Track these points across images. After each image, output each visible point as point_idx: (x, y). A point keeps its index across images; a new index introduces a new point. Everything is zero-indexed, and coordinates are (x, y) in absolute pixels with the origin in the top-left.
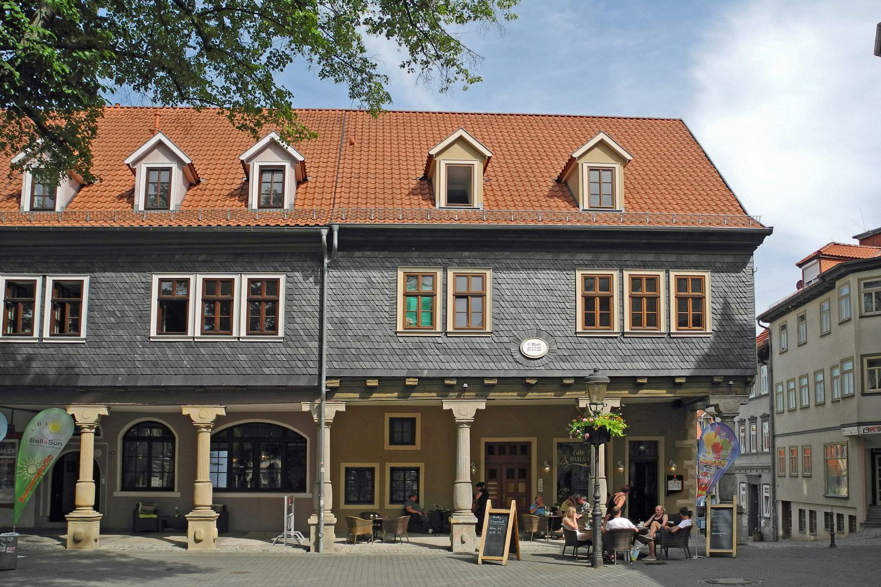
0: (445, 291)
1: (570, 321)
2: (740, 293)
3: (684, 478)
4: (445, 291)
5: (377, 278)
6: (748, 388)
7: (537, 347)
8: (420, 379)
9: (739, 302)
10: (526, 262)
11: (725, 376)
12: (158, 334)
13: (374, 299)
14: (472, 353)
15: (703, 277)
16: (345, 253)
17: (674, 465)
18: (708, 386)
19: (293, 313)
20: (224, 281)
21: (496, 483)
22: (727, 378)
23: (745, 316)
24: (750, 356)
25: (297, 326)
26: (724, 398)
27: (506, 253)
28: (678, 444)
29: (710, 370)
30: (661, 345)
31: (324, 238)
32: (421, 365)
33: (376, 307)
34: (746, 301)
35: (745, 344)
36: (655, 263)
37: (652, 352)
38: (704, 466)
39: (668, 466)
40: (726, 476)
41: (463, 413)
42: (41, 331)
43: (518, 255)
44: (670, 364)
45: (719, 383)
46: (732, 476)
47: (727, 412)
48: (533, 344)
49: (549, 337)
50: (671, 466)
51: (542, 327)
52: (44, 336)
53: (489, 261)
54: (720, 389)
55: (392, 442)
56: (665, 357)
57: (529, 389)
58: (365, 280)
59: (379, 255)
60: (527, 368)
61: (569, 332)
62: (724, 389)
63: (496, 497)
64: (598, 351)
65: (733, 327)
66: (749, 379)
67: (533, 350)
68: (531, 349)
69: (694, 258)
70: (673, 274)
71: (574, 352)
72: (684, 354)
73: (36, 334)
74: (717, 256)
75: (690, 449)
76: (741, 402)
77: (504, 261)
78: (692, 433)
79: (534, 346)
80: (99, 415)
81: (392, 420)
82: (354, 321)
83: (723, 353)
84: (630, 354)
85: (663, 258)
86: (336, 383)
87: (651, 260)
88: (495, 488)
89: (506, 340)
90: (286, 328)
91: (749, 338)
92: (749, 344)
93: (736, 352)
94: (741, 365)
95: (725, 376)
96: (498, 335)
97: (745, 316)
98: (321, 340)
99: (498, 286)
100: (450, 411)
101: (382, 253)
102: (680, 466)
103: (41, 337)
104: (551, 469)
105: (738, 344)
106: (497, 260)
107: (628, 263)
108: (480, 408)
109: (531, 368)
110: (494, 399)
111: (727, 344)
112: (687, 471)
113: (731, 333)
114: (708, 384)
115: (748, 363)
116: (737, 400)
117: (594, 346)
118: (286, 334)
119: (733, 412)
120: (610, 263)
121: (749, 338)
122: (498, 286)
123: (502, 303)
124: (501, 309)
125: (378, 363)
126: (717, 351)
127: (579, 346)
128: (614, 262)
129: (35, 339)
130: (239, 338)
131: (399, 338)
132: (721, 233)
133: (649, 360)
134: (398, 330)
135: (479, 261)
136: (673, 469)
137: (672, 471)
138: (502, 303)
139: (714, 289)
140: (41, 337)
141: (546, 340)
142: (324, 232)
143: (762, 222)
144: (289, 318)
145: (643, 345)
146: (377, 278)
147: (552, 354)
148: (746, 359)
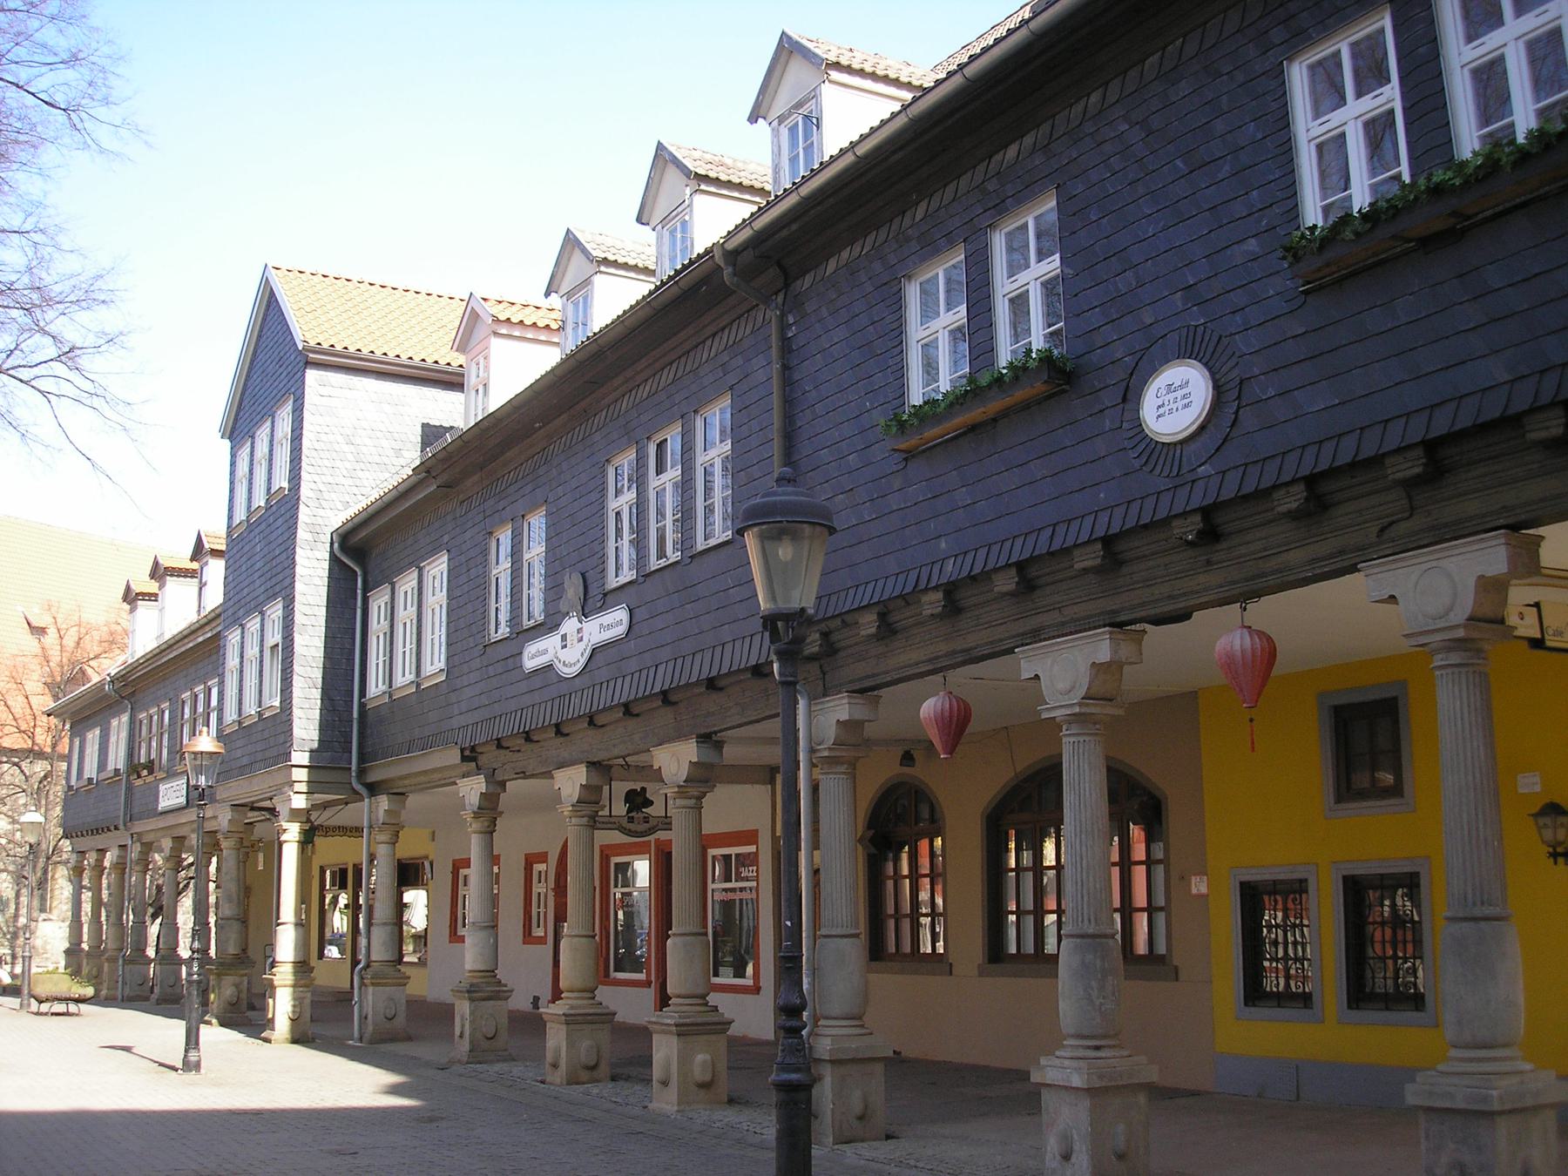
7: (1180, 393)
68: (1166, 408)
79: (1171, 396)
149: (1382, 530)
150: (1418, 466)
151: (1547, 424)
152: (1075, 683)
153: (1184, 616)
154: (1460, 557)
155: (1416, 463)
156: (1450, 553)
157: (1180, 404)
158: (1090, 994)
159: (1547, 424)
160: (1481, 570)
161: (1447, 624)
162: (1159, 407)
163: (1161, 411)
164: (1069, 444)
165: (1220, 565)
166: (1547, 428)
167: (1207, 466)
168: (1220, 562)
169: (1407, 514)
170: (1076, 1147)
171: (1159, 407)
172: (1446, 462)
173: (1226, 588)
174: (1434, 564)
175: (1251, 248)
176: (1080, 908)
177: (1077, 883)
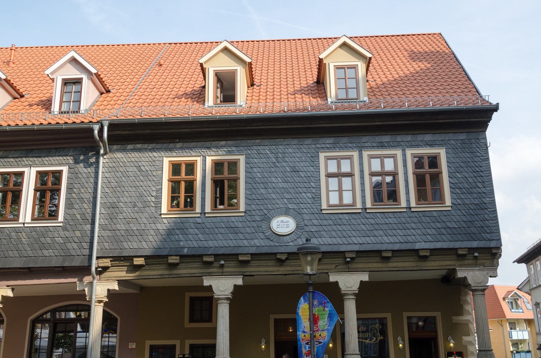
1: (316, 199)
2: (476, 168)
3: (465, 355)
5: (146, 167)
7: (285, 224)
8: (182, 257)
9: (476, 175)
10: (275, 148)
11: (469, 248)
12: (212, 210)
13: (142, 185)
14: (228, 232)
15: (396, 155)
16: (119, 146)
17: (452, 341)
18: (164, 267)
19: (72, 200)
20: (54, 172)
22: (471, 250)
23: (483, 189)
24: (492, 228)
25: (75, 212)
26: (472, 270)
27: (257, 141)
28: (455, 319)
29: (453, 243)
30: (403, 219)
31: (96, 132)
32: (182, 243)
33: (144, 192)
34: (482, 175)
35: (486, 216)
36: (391, 143)
37: (394, 226)
38: (306, 344)
39: (447, 341)
40: (483, 352)
41: (221, 289)
42: (408, 201)
43: (266, 142)
44: (413, 237)
45: (464, 256)
46: (489, 352)
47: (477, 285)
48: (282, 221)
49: (297, 214)
50: (449, 343)
51: (290, 206)
52: (206, 211)
53: (242, 148)
54: (467, 262)
55: (192, 320)
56: (408, 231)
57: (281, 265)
58: (135, 169)
59: (148, 146)
60: (277, 244)
61: (315, 210)
62: (470, 262)
64: (398, 225)
65: (472, 200)
66: (494, 251)
67: (282, 227)
68: (280, 226)
69: (428, 137)
70: (409, 152)
71: (320, 228)
72: (426, 227)
73: (198, 209)
74: (450, 134)
75: (467, 325)
76: (490, 275)
77: (255, 147)
78: (467, 309)
79: (283, 224)
80: (109, 290)
81: (192, 299)
82: (124, 205)
83: (465, 226)
84: (373, 229)
85: (399, 138)
86: (107, 262)
87: (388, 141)
89: (258, 218)
90: (66, 213)
91: (489, 210)
92: (491, 216)
93: (478, 224)
95: (469, 248)
96: (251, 214)
97: (483, 189)
98: (93, 223)
99: (250, 170)
100: (336, 283)
101: (151, 145)
102: (458, 341)
103: (203, 213)
104: (404, 345)
105: (479, 216)
106: (249, 147)
107: (366, 145)
108: (364, 280)
109: (281, 245)
110: (253, 275)
111: (467, 216)
112: (466, 347)
114: (378, 259)
116: (485, 273)
117: (339, 221)
118: (65, 218)
119: (482, 284)
120: (350, 145)
121: (489, 210)
122: (250, 170)
123: (254, 185)
124: (253, 190)
125: (144, 243)
126: (458, 223)
127: (325, 222)
128: (354, 144)
129: (60, 223)
130: (24, 224)
131: (163, 219)
133: (392, 234)
134: (162, 212)
135: (234, 149)
136: (452, 345)
137: (451, 347)
138: (254, 185)
139: (450, 165)
140: (203, 213)
141: (294, 218)
142: (96, 128)
143: (490, 101)
144: (69, 205)
145: (386, 220)
146: (146, 167)
147: (300, 230)
148: (489, 231)
149: (335, 267)
163: (278, 226)
174: (349, 276)
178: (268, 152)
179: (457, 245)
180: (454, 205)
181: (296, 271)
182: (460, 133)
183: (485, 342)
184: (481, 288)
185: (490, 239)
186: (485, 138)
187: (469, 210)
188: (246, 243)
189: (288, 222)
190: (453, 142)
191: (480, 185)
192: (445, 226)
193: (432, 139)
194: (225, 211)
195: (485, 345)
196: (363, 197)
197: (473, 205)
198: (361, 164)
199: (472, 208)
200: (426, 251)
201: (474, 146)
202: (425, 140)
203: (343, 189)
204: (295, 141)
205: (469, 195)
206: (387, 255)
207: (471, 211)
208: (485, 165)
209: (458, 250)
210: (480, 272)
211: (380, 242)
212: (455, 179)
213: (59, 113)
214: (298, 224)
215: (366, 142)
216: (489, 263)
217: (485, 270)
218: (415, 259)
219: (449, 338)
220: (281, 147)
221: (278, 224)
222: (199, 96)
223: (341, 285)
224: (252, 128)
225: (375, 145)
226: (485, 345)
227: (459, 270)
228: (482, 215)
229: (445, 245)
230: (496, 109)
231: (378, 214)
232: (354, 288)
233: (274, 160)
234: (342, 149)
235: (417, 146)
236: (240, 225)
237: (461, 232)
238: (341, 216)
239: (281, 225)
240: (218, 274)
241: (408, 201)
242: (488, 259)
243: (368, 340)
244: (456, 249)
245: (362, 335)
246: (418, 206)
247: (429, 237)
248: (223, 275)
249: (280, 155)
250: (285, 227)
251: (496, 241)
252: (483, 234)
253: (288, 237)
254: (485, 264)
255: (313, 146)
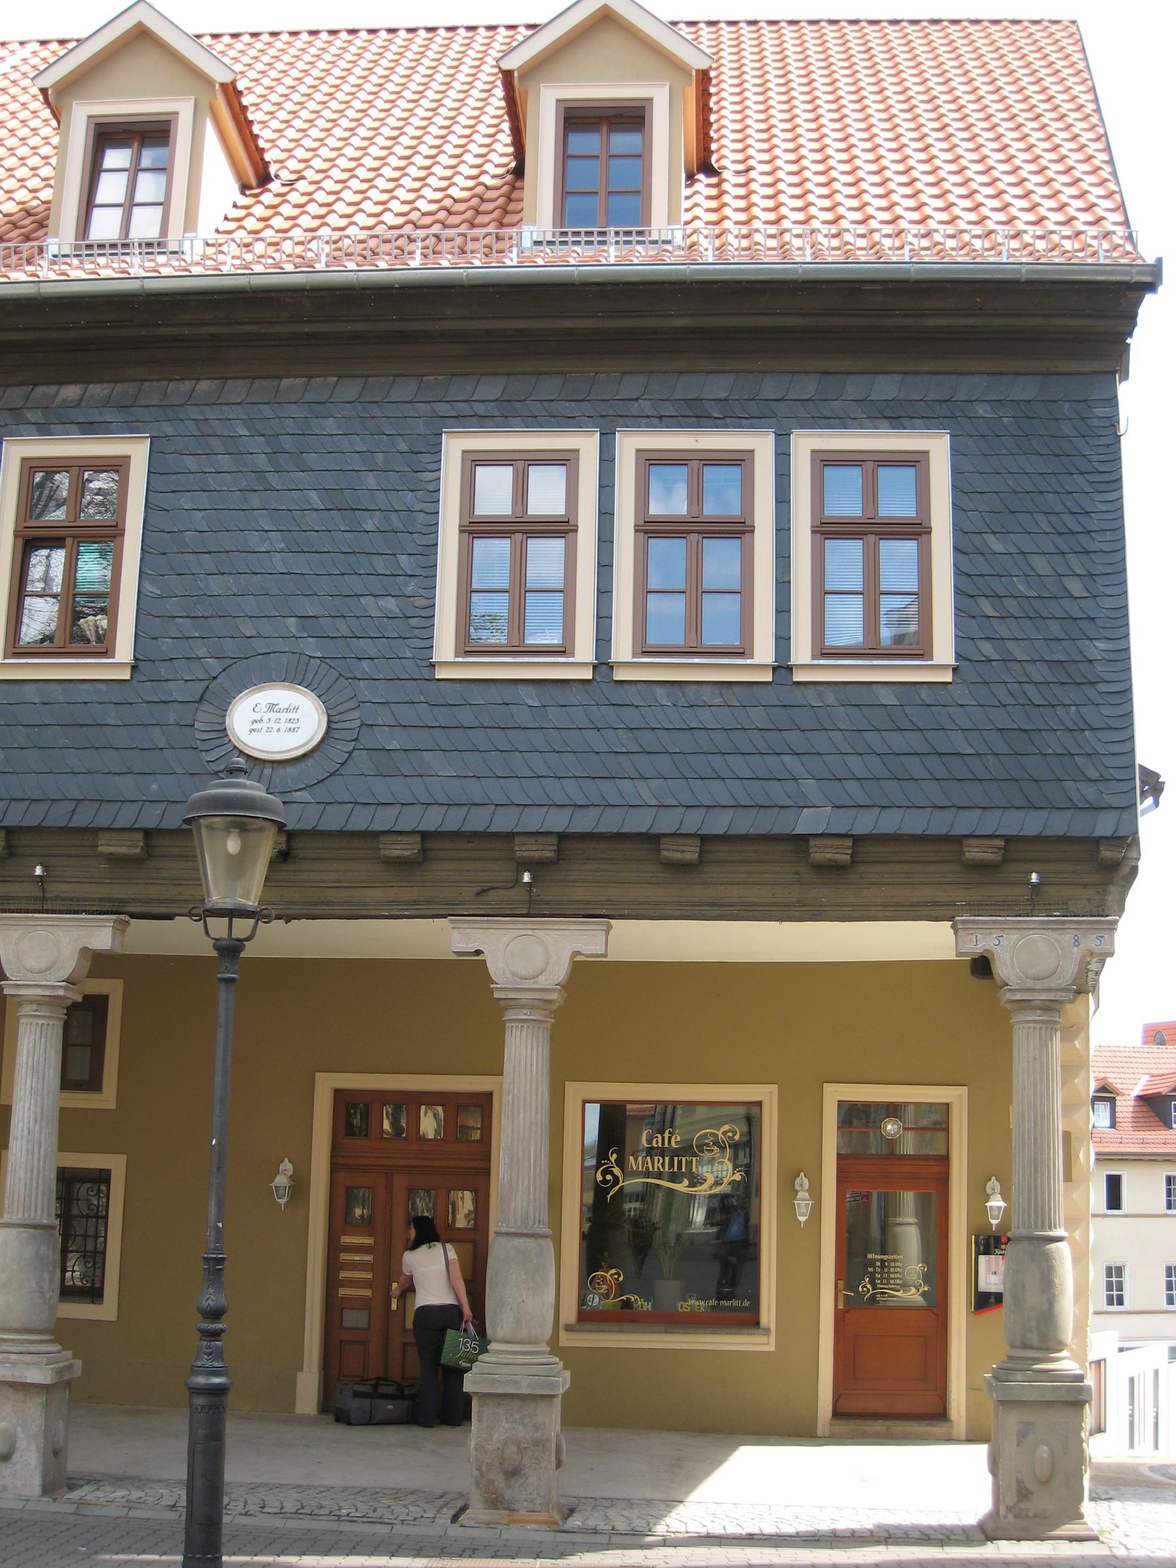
0: (605, 540)
4: (605, 540)
6: (1112, 889)
7: (284, 716)
21: (369, 1241)
35: (1089, 712)
39: (979, 1196)
42: (783, 639)
45: (835, 868)
47: (1030, 983)
48: (272, 707)
63: (367, 1293)
65: (1039, 645)
66: (1106, 853)
67: (269, 730)
68: (265, 725)
69: (886, 388)
71: (422, 738)
79: (273, 716)
83: (1001, 747)
85: (770, 388)
87: (723, 395)
88: (368, 1258)
91: (1103, 687)
94: (1074, 795)
113: (1030, 668)
115: (1101, 785)
121: (1103, 687)
132: (615, 284)
148: (1093, 773)
149: (479, 894)
150: (551, 851)
151: (684, 848)
152: (54, 963)
153: (170, 917)
154: (558, 932)
155: (547, 847)
156: (551, 927)
157: (283, 726)
158: (42, 1288)
159: (684, 848)
160: (577, 946)
161: (535, 986)
162: (255, 721)
163: (256, 726)
164: (112, 723)
165: (277, 884)
166: (683, 852)
167: (305, 792)
168: (280, 881)
169: (511, 885)
170: (22, 1444)
171: (255, 721)
172: (568, 852)
173: (281, 907)
174: (529, 932)
175: (390, 606)
176: (33, 1197)
177: (32, 1171)
178: (243, 431)
179: (964, 823)
180: (967, 663)
181: (323, 903)
182: (1017, 374)
183: (1036, 1204)
184: (1044, 996)
185: (1096, 805)
186: (1113, 401)
187: (1025, 686)
188: (127, 786)
189: (296, 709)
190: (981, 410)
191: (1075, 587)
192: (922, 747)
193: (902, 396)
194: (696, 660)
195: (1037, 1217)
196: (603, 618)
197: (1043, 667)
198: (606, 486)
199: (1037, 677)
200: (838, 842)
201: (1067, 429)
202: (873, 397)
203: (529, 586)
204: (350, 390)
205: (1027, 624)
206: (678, 856)
207: (1031, 691)
208: (1104, 509)
209: (812, 842)
210: (1050, 933)
211: (654, 802)
212: (979, 560)
213: (77, 247)
214: (337, 718)
215: (636, 400)
216: (1089, 900)
217: (1066, 926)
218: (798, 873)
219: (989, 1184)
220: (294, 410)
221: (257, 717)
222: (511, 192)
223: (497, 967)
224: (176, 331)
225: (669, 410)
226: (1037, 1217)
227: (964, 922)
228: (1073, 709)
229: (915, 823)
230: (1147, 279)
231: (659, 691)
232: (544, 981)
233: (262, 462)
234: (534, 421)
235: (841, 421)
236: (111, 716)
237: (982, 773)
238: (508, 694)
239: (265, 720)
240: (23, 907)
241: (783, 639)
242: (1085, 886)
243: (686, 1182)
244: (959, 839)
245: (663, 1165)
246: (822, 662)
247: (852, 786)
248: (42, 912)
249: (287, 443)
250: (283, 729)
251: (1115, 814)
252: (1069, 784)
253: (290, 770)
254: (1070, 903)
255: (423, 408)
